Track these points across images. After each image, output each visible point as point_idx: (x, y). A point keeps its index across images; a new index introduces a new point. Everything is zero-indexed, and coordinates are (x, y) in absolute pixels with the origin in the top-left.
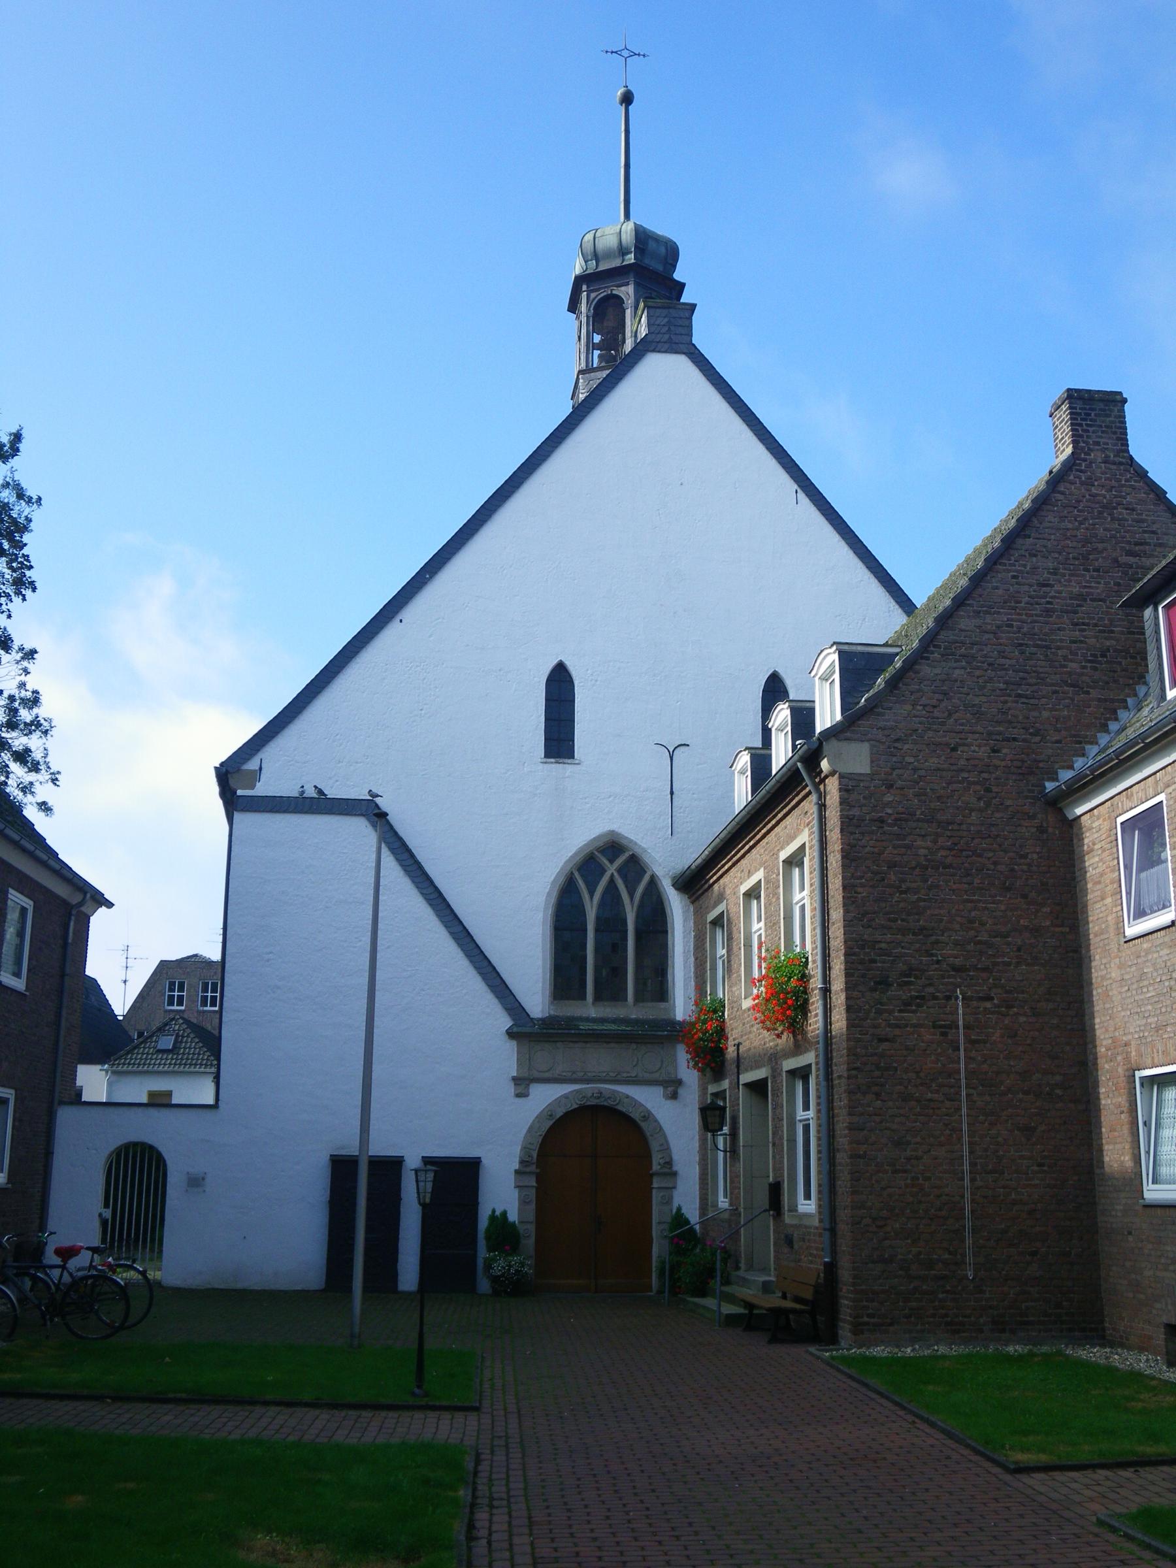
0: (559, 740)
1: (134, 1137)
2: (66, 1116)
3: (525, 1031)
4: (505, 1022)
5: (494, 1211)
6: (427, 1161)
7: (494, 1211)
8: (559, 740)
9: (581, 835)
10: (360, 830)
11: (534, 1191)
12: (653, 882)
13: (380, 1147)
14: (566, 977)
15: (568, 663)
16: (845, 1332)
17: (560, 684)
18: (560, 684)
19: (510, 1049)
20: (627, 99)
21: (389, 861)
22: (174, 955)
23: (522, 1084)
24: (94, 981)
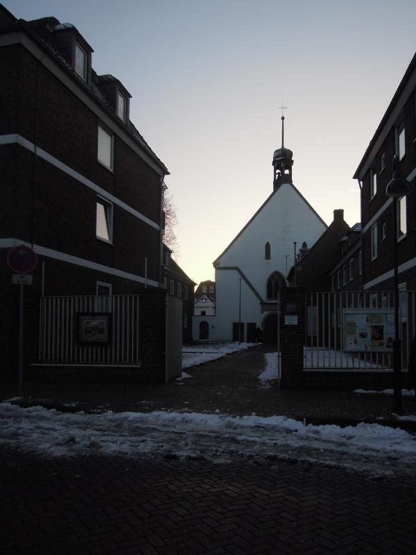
0: (268, 256)
1: (204, 320)
2: (193, 317)
3: (262, 303)
4: (259, 302)
5: (305, 245)
6: (248, 324)
7: (305, 245)
8: (268, 256)
9: (272, 271)
10: (235, 271)
11: (325, 230)
12: (284, 279)
13: (242, 322)
14: (269, 296)
15: (270, 243)
16: (381, 324)
17: (268, 246)
18: (268, 246)
19: (260, 306)
20: (283, 118)
21: (243, 282)
22: (203, 281)
23: (262, 311)
24: (21, 20)
